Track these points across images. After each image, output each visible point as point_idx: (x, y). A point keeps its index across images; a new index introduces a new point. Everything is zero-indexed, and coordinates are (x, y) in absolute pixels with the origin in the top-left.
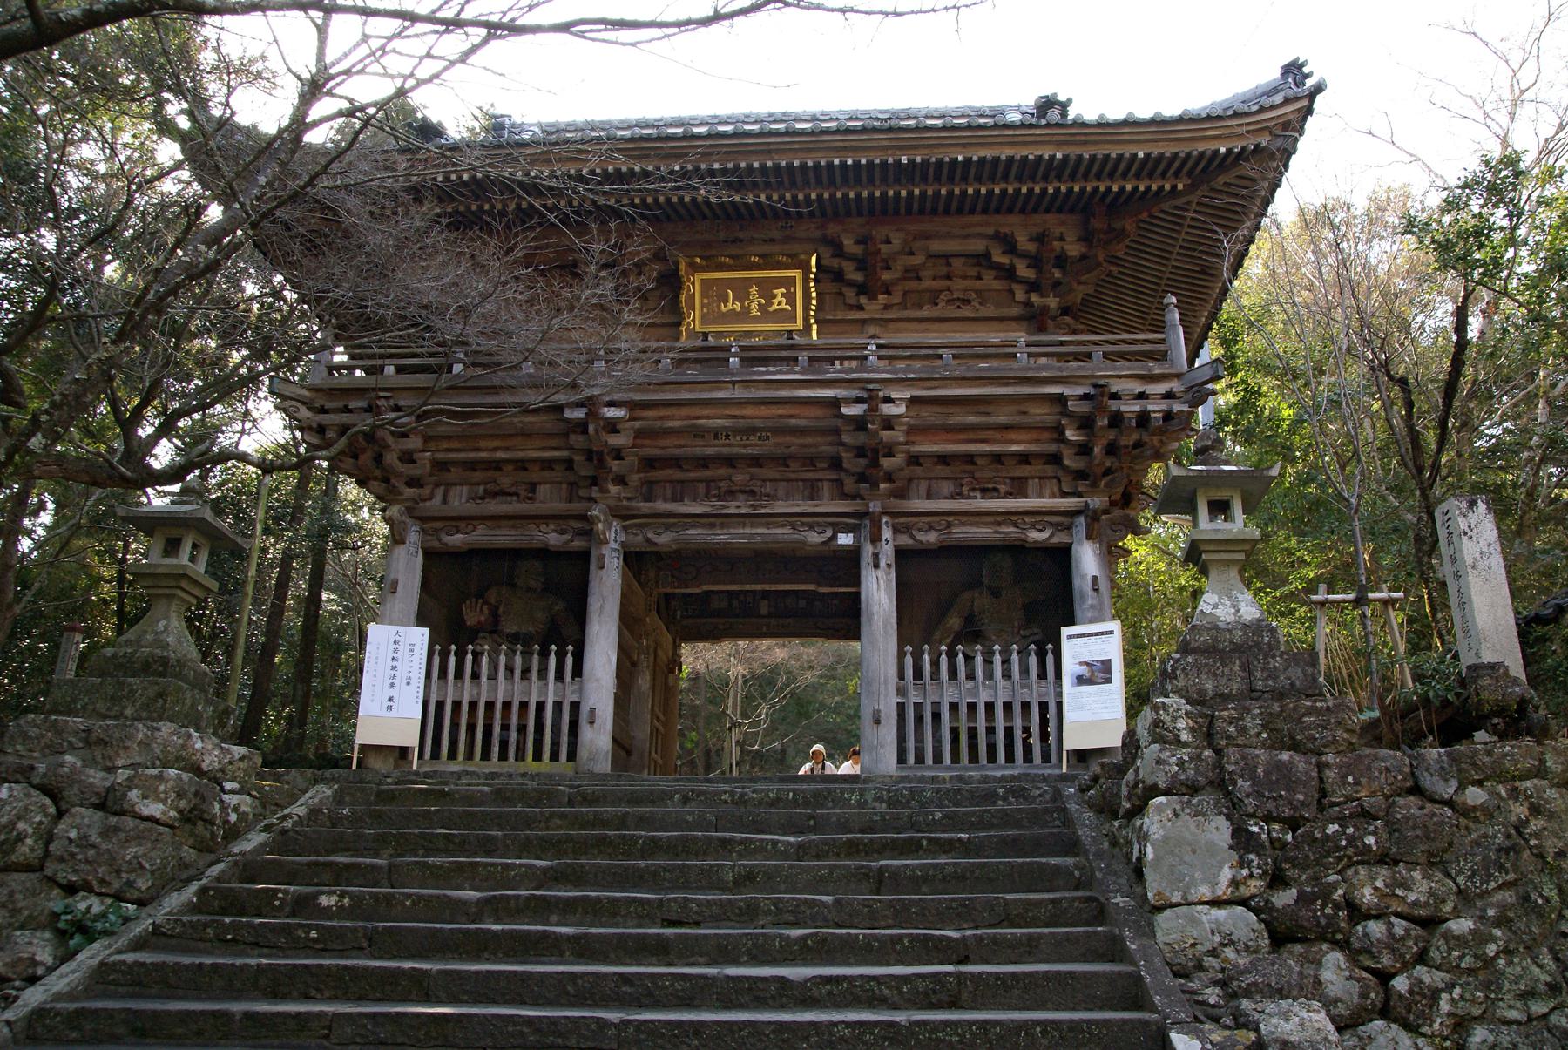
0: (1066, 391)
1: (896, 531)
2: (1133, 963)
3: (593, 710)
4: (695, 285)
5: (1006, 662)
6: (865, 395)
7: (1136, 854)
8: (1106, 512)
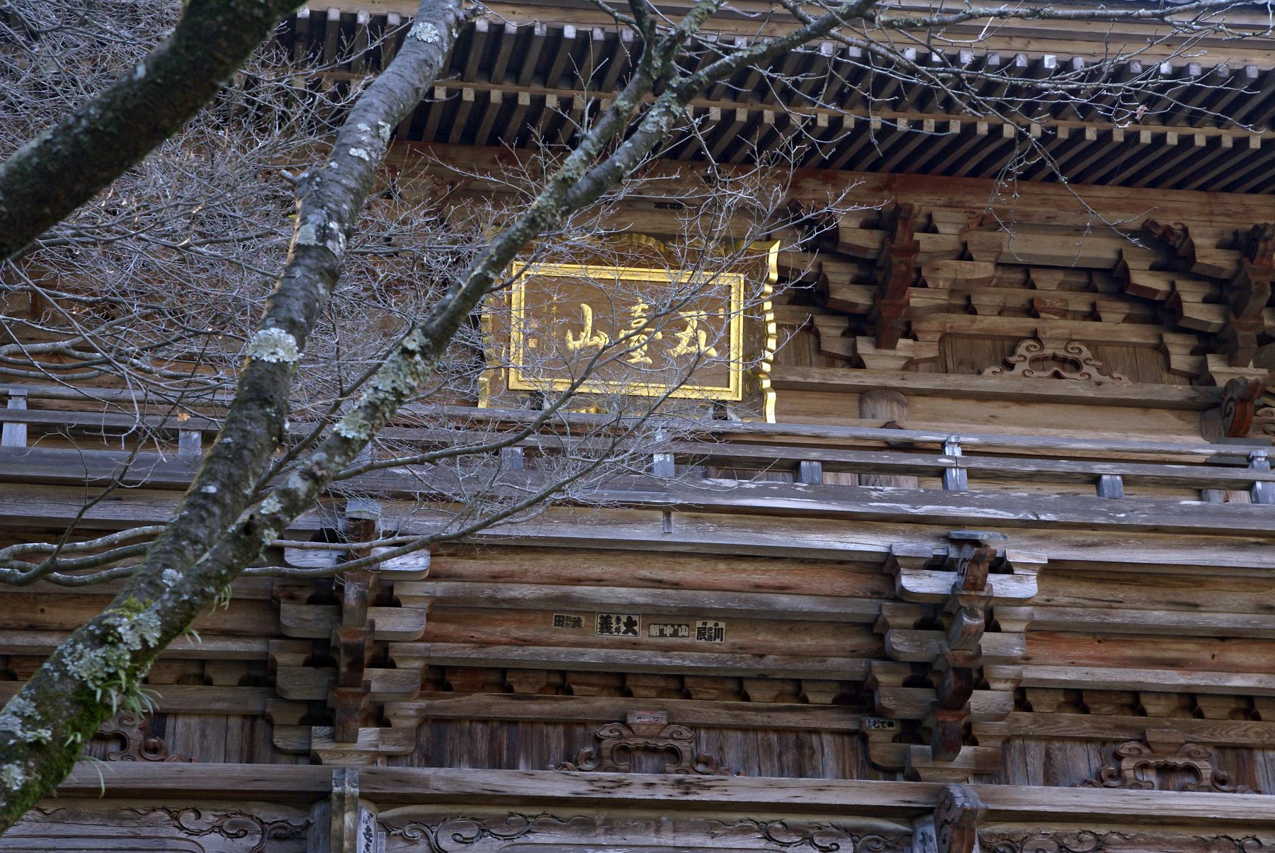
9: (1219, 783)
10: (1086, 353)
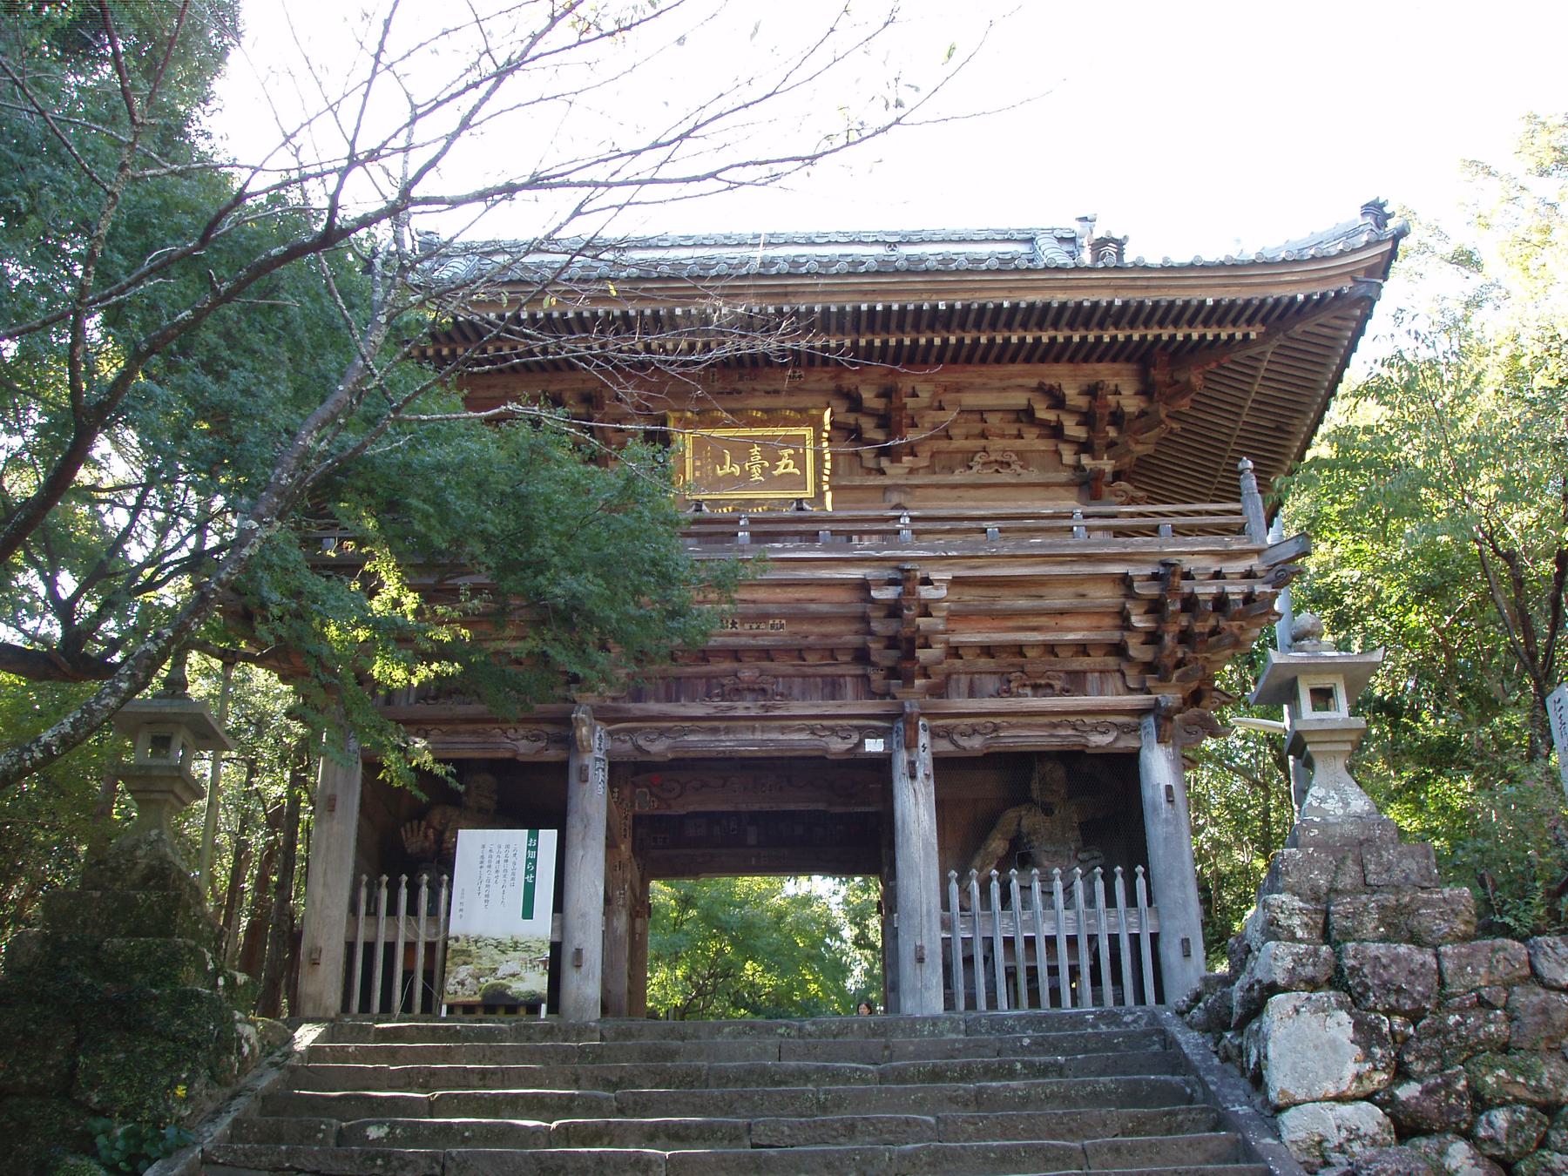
0: (1132, 570)
1: (935, 734)
2: (1265, 1161)
3: (579, 952)
4: (685, 440)
5: (1068, 891)
6: (898, 576)
7: (1253, 1059)
8: (1179, 711)
9: (1065, 692)
10: (1014, 457)
